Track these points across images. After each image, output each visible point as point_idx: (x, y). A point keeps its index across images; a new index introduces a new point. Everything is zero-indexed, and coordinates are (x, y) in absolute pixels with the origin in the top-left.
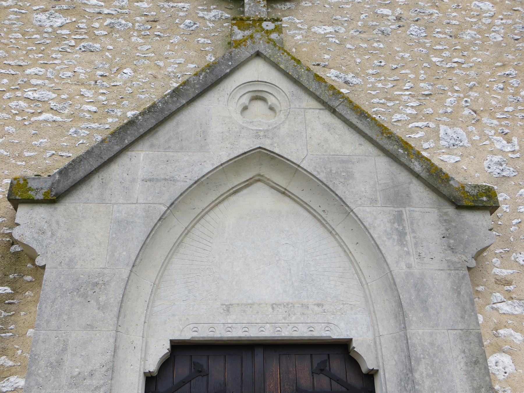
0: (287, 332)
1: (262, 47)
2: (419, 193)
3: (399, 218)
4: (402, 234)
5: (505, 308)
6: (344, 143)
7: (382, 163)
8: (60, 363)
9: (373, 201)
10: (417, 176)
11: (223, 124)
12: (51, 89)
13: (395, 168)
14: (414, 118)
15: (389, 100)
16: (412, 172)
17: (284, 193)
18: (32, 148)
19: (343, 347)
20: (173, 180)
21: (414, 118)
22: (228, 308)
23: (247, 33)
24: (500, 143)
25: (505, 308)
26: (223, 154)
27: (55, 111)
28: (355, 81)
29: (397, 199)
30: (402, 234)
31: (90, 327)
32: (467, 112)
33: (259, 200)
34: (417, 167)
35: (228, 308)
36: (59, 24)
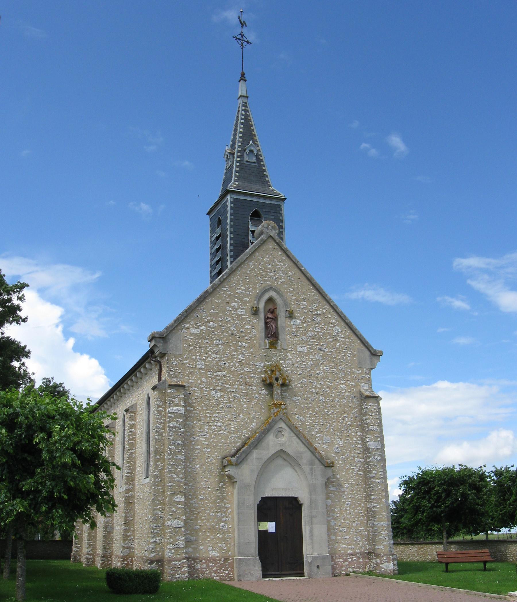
0: (285, 495)
1: (282, 416)
2: (317, 461)
3: (312, 469)
4: (312, 473)
5: (332, 489)
6: (302, 448)
7: (309, 453)
8: (244, 503)
9: (306, 465)
10: (317, 458)
11: (273, 443)
12: (221, 422)
13: (312, 455)
14: (318, 433)
15: (311, 426)
16: (316, 457)
17: (285, 460)
18: (220, 443)
19: (296, 499)
20: (261, 459)
21: (318, 433)
22: (273, 490)
23: (277, 409)
24: (339, 442)
25: (332, 489)
26: (273, 452)
27: (224, 431)
28: (303, 419)
29: (312, 464)
30: (312, 473)
31: (249, 495)
32: (332, 430)
33: (280, 461)
34: (317, 455)
35: (273, 490)
36: (219, 396)
